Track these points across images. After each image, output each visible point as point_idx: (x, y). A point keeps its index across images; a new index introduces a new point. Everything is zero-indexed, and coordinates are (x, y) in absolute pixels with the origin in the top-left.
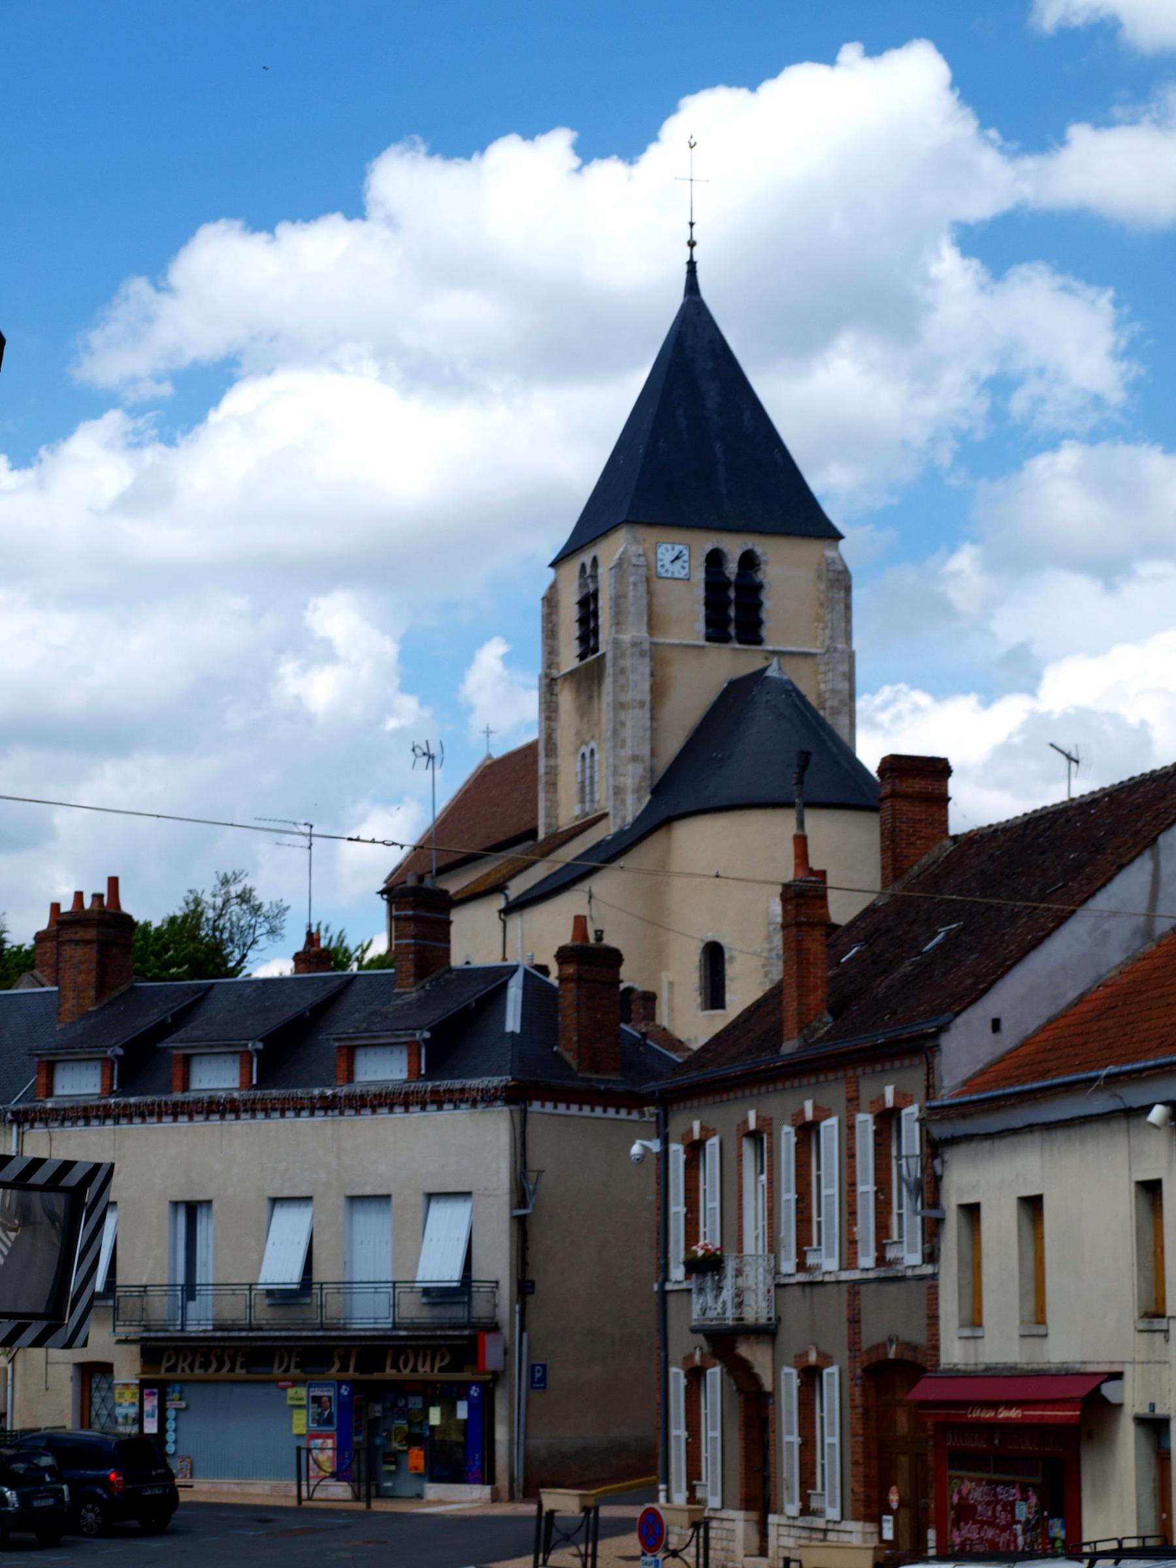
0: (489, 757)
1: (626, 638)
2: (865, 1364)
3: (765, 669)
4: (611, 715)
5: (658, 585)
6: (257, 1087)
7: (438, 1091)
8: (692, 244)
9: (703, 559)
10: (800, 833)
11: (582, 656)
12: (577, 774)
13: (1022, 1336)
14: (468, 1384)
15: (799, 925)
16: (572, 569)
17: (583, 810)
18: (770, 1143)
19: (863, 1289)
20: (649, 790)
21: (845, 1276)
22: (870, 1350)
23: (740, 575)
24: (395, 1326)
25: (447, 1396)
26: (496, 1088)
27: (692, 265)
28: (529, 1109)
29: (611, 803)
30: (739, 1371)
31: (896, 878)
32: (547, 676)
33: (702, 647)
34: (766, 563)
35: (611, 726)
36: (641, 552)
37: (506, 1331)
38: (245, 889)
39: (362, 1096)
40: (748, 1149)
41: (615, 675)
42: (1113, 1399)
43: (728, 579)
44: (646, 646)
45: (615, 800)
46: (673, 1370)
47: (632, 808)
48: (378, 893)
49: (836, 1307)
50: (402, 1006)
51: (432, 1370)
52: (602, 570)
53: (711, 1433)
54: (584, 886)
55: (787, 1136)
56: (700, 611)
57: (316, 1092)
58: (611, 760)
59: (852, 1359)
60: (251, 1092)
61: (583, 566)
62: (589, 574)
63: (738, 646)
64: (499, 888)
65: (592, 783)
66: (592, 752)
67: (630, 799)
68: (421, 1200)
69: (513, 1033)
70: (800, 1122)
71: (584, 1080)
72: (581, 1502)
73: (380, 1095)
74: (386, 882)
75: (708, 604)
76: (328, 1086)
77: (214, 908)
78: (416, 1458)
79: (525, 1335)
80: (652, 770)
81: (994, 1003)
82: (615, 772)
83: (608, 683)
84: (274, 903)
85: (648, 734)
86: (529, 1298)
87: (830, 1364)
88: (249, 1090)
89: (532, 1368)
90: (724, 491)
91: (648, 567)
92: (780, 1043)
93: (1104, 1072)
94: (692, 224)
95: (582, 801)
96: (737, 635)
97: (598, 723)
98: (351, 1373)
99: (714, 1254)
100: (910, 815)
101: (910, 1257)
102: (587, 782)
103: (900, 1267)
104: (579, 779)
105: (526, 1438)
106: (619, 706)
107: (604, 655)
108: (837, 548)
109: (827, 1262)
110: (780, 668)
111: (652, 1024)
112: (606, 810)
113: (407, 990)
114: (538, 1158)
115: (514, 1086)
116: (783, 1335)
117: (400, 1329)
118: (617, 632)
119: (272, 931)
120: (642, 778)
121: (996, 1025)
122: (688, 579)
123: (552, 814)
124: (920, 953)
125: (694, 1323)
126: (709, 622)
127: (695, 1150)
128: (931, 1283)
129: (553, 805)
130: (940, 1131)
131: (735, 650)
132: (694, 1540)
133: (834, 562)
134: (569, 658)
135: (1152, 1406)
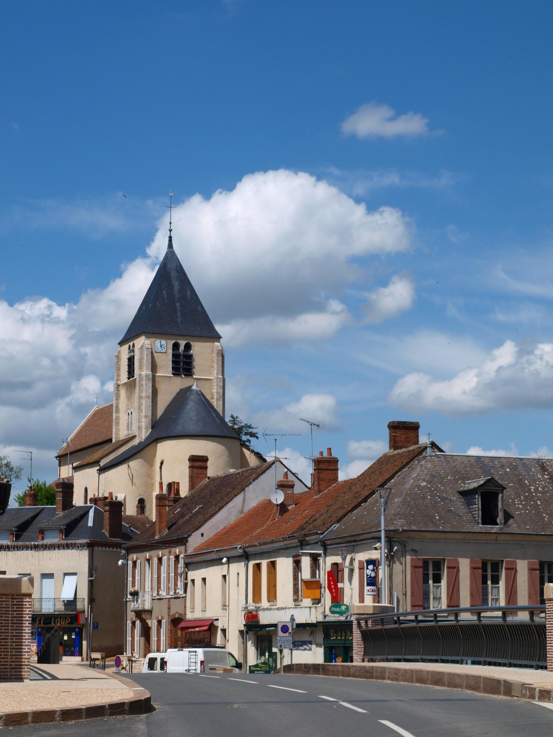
1: (144, 373)
2: (171, 619)
3: (192, 386)
4: (138, 401)
6: (15, 541)
7: (68, 544)
8: (171, 231)
9: (172, 345)
10: (161, 481)
11: (129, 378)
12: (126, 420)
13: (202, 611)
14: (75, 628)
15: (160, 506)
16: (126, 347)
17: (128, 432)
18: (152, 562)
19: (171, 600)
20: (151, 427)
21: (167, 597)
22: (172, 616)
23: (184, 351)
25: (69, 632)
26: (84, 543)
27: (170, 238)
28: (94, 549)
29: (137, 432)
30: (143, 622)
31: (192, 489)
33: (171, 377)
34: (194, 347)
35: (138, 404)
36: (149, 343)
37: (86, 612)
38: (7, 462)
39: (46, 545)
41: (139, 387)
42: (216, 625)
45: (139, 431)
46: (128, 622)
47: (143, 435)
48: (55, 457)
49: (165, 603)
50: (58, 518)
51: (65, 624)
52: (136, 349)
53: (137, 638)
55: (155, 561)
57: (33, 543)
58: (138, 417)
59: (168, 618)
60: (13, 543)
62: (131, 350)
65: (131, 424)
67: (144, 430)
68: (62, 575)
69: (90, 527)
70: (158, 557)
71: (110, 540)
72: (101, 656)
73: (51, 544)
76: (36, 541)
78: (61, 649)
79: (92, 614)
82: (139, 421)
83: (137, 388)
84: (18, 467)
87: (164, 619)
88: (13, 542)
89: (94, 623)
92: (154, 536)
93: (216, 550)
94: (170, 223)
95: (128, 430)
97: (134, 403)
98: (42, 625)
99: (137, 591)
100: (197, 472)
101: (180, 592)
102: (130, 423)
103: (179, 595)
104: (127, 422)
105: (92, 643)
106: (140, 398)
107: (136, 379)
109: (163, 593)
110: (197, 386)
111: (143, 515)
112: (136, 434)
113: (60, 513)
115: (89, 543)
117: (56, 612)
118: (141, 371)
119: (17, 477)
120: (148, 424)
121: (202, 535)
122: (166, 353)
123: (117, 434)
124: (192, 513)
125: (132, 609)
126: (173, 368)
127: (135, 563)
129: (118, 430)
130: (187, 561)
132: (129, 665)
135: (223, 626)
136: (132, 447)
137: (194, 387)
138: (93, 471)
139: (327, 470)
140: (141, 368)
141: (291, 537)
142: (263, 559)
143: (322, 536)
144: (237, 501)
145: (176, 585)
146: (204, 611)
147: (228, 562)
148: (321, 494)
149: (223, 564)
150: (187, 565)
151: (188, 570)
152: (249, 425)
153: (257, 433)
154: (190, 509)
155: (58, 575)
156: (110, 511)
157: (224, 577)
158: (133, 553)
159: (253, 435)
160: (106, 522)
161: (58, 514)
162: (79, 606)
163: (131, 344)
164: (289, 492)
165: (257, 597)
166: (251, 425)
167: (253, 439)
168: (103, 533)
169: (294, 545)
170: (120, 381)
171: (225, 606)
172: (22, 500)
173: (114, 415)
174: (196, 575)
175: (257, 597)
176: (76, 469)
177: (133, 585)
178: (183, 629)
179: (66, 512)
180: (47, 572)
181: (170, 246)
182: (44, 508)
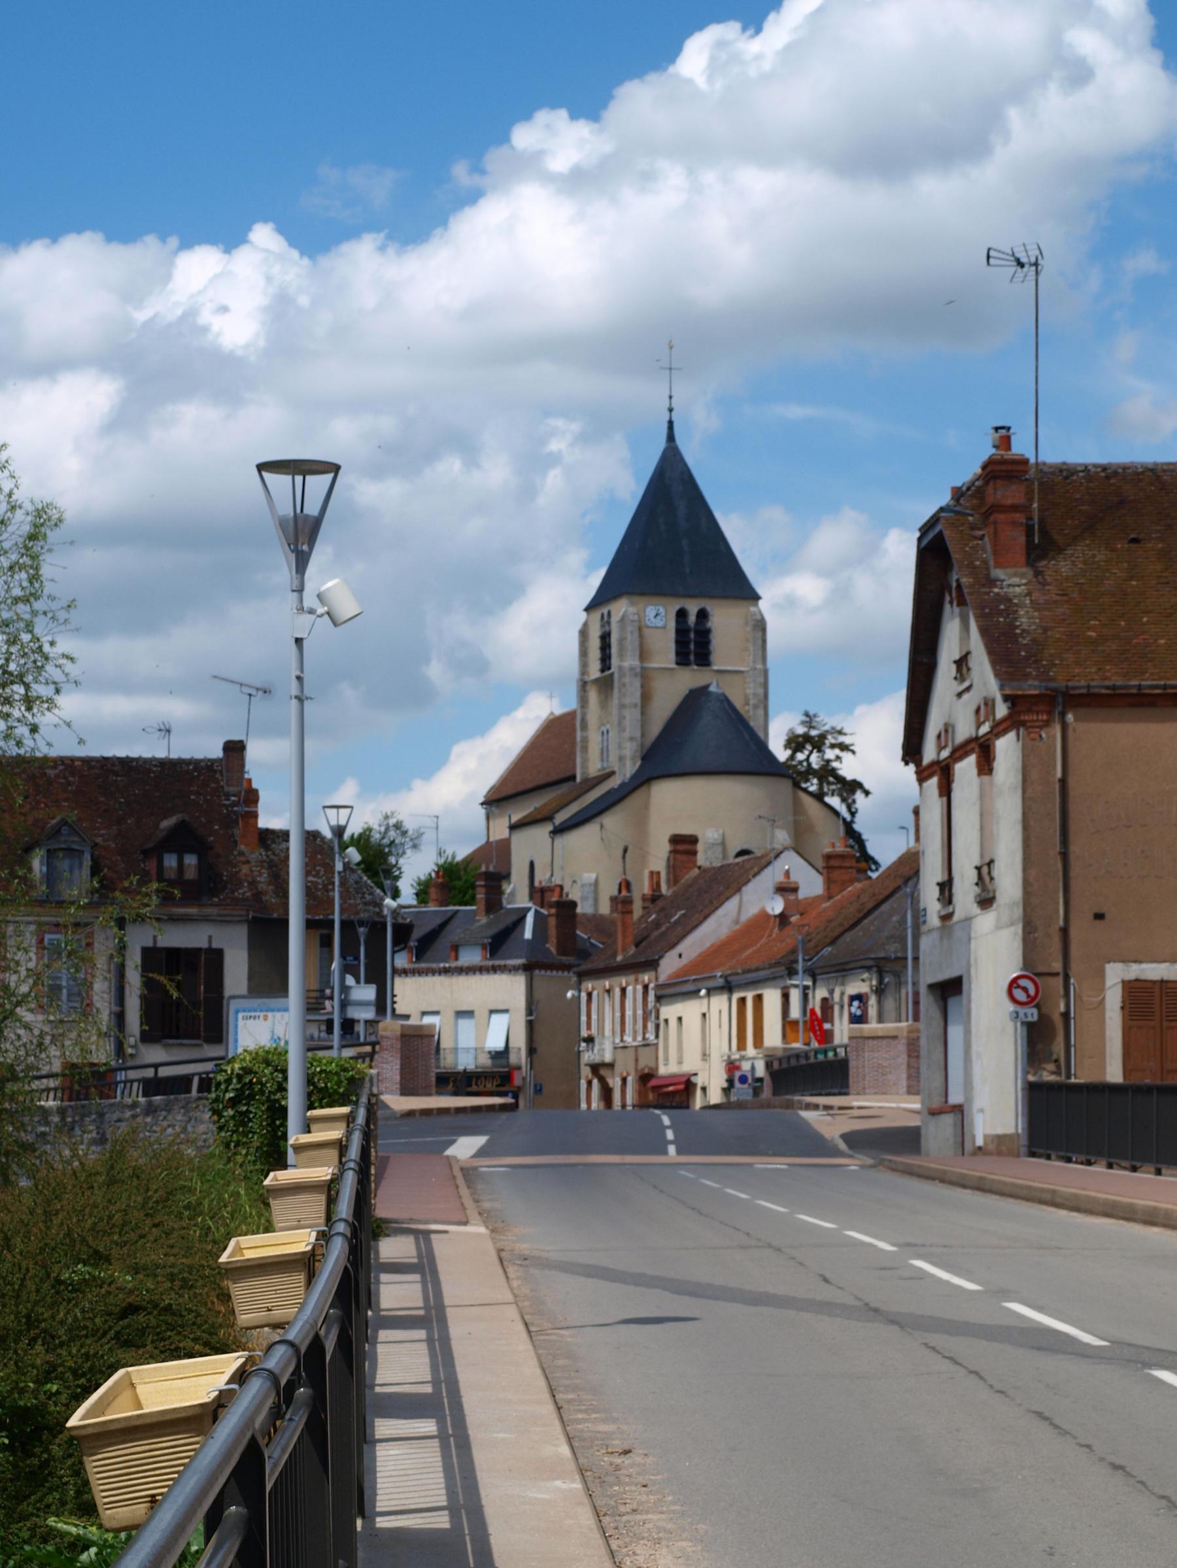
0: (552, 713)
1: (626, 664)
5: (646, 631)
6: (415, 962)
11: (602, 671)
16: (596, 616)
17: (602, 765)
24: (476, 1067)
27: (671, 424)
30: (602, 1080)
32: (582, 680)
33: (672, 669)
37: (524, 1069)
40: (606, 995)
43: (688, 626)
44: (638, 670)
47: (628, 769)
49: (630, 1054)
54: (598, 820)
55: (617, 992)
56: (672, 646)
57: (442, 965)
61: (603, 615)
62: (606, 621)
63: (695, 667)
64: (549, 818)
65: (608, 750)
66: (608, 731)
67: (628, 763)
68: (487, 1013)
74: (485, 797)
75: (677, 642)
76: (447, 962)
77: (380, 833)
80: (642, 745)
81: (682, 947)
82: (620, 747)
83: (616, 690)
85: (639, 724)
86: (535, 1056)
89: (535, 1086)
90: (687, 570)
91: (639, 621)
94: (671, 397)
95: (602, 760)
96: (695, 660)
101: (651, 1036)
106: (622, 706)
108: (757, 605)
109: (628, 1039)
114: (538, 994)
116: (616, 1067)
119: (415, 846)
121: (680, 956)
126: (678, 654)
127: (589, 995)
128: (657, 1045)
129: (585, 761)
130: (660, 993)
131: (694, 670)
133: (755, 614)
134: (594, 672)
136: (609, 792)
137: (713, 689)
138: (541, 833)
139: (840, 867)
140: (621, 656)
141: (777, 964)
142: (748, 990)
143: (809, 963)
144: (731, 906)
145: (645, 1027)
146: (680, 1062)
147: (709, 994)
148: (832, 901)
149: (701, 997)
150: (659, 998)
151: (661, 1005)
152: (839, 728)
153: (852, 745)
154: (668, 916)
155: (481, 1013)
156: (557, 915)
157: (704, 1015)
158: (589, 979)
159: (844, 747)
160: (552, 932)
161: (478, 921)
162: (513, 1059)
163: (605, 611)
164: (792, 897)
165: (742, 1045)
166: (842, 729)
167: (846, 756)
168: (548, 949)
169: (781, 974)
170: (588, 675)
171: (705, 1056)
172: (423, 891)
173: (579, 734)
174: (669, 1011)
175: (742, 1045)
176: (513, 827)
177: (589, 1027)
178: (656, 1088)
179: (491, 916)
180: (464, 1008)
181: (671, 437)
182: (457, 912)
